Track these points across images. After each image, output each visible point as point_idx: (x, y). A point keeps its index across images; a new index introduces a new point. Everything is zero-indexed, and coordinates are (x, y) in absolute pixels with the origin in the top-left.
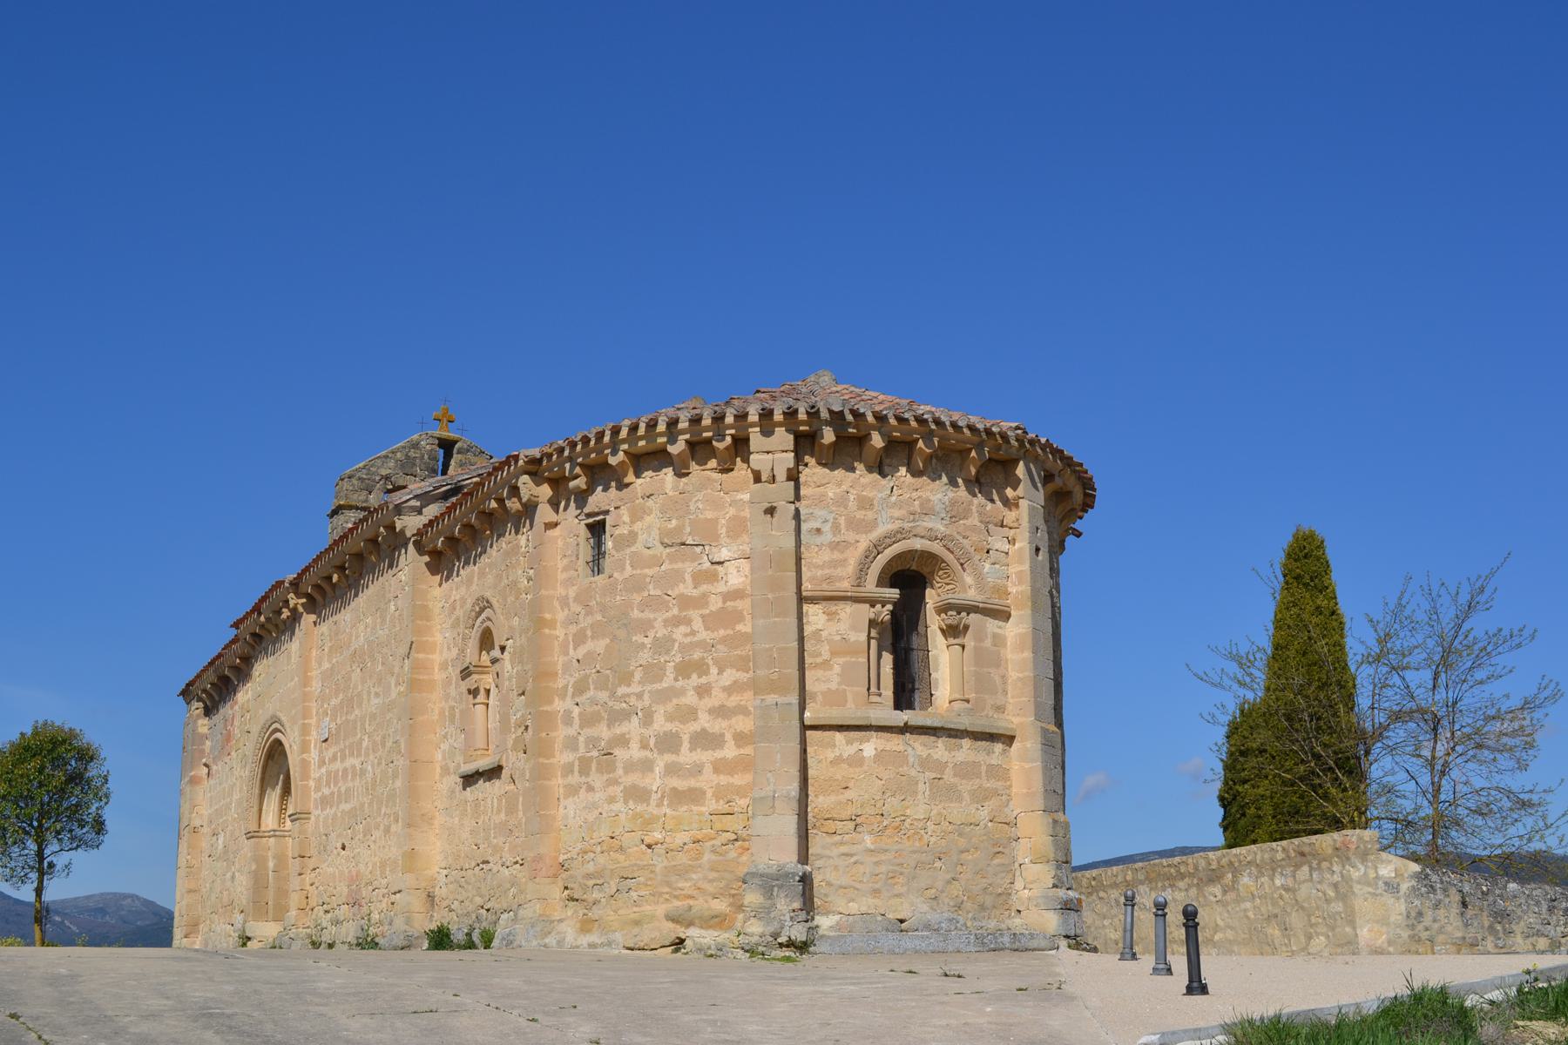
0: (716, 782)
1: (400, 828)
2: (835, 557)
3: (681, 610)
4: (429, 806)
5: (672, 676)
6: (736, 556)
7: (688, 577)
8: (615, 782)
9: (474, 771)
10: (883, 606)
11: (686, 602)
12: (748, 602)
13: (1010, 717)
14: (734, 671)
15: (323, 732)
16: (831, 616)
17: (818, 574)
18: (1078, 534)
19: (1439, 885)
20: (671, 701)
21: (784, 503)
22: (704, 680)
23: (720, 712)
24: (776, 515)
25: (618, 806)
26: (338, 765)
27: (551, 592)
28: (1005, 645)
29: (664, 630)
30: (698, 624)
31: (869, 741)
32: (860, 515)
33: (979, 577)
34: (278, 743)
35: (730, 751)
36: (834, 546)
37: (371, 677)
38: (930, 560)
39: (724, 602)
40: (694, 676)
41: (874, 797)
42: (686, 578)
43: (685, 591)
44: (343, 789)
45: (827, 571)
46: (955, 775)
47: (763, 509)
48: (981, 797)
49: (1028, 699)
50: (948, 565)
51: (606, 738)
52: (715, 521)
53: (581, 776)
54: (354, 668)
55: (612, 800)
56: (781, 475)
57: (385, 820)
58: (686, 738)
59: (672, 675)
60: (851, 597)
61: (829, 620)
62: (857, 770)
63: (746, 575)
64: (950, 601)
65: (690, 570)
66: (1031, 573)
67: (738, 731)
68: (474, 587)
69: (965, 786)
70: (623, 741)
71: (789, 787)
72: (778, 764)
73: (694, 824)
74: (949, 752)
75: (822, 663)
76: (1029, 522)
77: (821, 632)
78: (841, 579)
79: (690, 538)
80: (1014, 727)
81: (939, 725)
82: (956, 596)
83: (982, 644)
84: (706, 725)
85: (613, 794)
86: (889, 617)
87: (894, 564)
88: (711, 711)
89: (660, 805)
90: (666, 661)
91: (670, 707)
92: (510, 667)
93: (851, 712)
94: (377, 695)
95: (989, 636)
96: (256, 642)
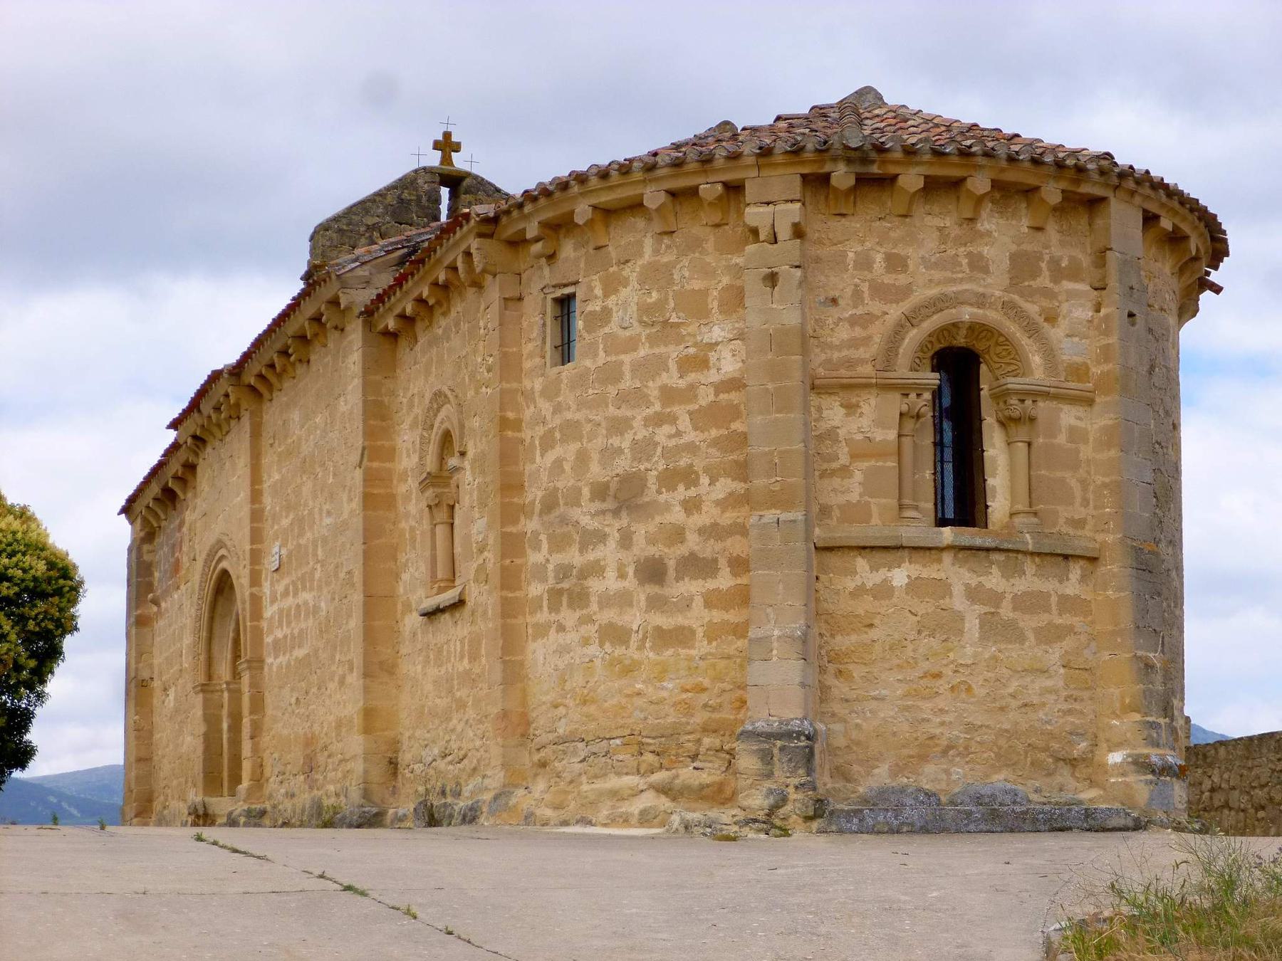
0: (707, 619)
1: (355, 679)
3: (663, 406)
4: (389, 651)
5: (654, 488)
7: (673, 366)
8: (589, 620)
9: (435, 607)
10: (919, 395)
11: (669, 395)
14: (729, 481)
15: (273, 559)
16: (851, 408)
18: (1217, 289)
20: (653, 519)
22: (692, 492)
25: (593, 649)
26: (290, 601)
27: (515, 385)
29: (644, 431)
30: (684, 423)
31: (899, 567)
32: (888, 279)
33: (1050, 354)
34: (225, 573)
36: (853, 321)
37: (322, 490)
39: (716, 395)
40: (681, 488)
42: (671, 367)
44: (296, 632)
45: (845, 353)
46: (1015, 609)
47: (761, 277)
50: (1007, 340)
51: (579, 565)
52: (705, 293)
53: (550, 613)
54: (305, 479)
55: (586, 642)
56: (784, 232)
57: (340, 669)
58: (671, 564)
60: (876, 384)
61: (847, 415)
63: (743, 360)
67: (735, 555)
68: (432, 379)
69: (1029, 623)
70: (596, 569)
72: (780, 597)
73: (681, 672)
84: (696, 548)
85: (586, 635)
88: (701, 531)
89: (641, 647)
90: (647, 470)
91: (652, 527)
92: (471, 479)
93: (877, 528)
94: (329, 513)
95: (1063, 430)
96: (198, 447)
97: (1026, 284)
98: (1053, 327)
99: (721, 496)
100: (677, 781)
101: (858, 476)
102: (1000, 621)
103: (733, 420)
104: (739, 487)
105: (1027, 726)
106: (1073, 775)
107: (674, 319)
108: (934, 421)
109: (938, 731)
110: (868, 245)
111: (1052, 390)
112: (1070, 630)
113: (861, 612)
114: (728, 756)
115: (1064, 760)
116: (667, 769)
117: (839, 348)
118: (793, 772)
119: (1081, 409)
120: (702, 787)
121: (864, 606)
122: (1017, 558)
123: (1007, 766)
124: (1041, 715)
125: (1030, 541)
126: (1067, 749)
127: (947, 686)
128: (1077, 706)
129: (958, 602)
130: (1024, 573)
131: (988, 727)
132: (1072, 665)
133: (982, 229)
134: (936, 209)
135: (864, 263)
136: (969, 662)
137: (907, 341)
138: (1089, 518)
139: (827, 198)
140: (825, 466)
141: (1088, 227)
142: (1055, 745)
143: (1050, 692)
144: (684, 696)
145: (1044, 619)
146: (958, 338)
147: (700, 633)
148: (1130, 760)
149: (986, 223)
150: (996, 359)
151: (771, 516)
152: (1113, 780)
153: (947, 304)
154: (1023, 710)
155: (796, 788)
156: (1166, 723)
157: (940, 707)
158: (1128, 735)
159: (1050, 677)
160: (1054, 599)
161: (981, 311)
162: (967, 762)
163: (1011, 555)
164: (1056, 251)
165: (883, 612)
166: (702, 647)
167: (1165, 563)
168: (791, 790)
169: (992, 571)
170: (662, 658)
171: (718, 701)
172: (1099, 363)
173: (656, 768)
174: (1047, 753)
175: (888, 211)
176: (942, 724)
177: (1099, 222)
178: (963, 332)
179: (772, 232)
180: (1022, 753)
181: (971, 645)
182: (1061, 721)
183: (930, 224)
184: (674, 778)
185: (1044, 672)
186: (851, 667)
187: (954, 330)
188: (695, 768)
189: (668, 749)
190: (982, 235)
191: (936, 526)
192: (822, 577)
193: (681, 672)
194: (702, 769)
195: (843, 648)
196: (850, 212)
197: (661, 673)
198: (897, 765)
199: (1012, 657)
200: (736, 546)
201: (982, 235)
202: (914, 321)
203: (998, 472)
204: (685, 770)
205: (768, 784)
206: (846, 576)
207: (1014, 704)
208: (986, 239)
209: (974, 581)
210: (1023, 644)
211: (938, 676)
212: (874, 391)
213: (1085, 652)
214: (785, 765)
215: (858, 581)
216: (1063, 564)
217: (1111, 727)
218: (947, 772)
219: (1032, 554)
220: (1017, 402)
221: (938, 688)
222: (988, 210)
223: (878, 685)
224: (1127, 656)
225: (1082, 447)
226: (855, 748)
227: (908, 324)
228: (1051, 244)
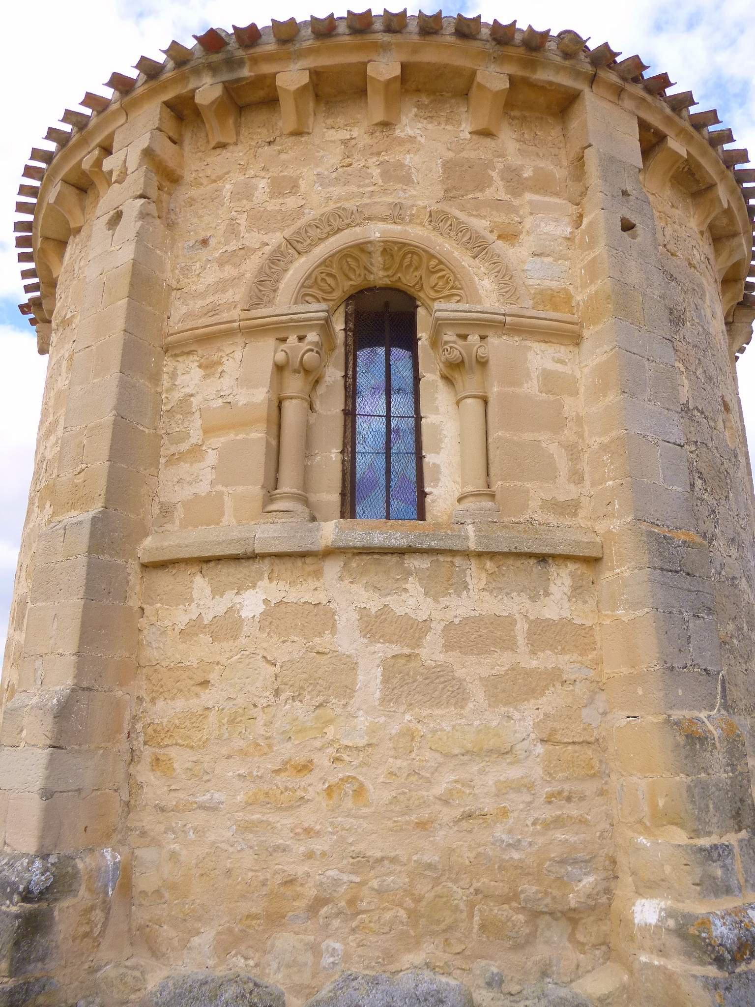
2: (225, 274)
10: (301, 339)
16: (210, 367)
31: (254, 587)
32: (273, 205)
49: (619, 482)
50: (441, 262)
60: (240, 329)
62: (226, 645)
74: (436, 600)
75: (189, 452)
77: (192, 399)
83: (517, 390)
95: (534, 376)
97: (470, 196)
98: (513, 245)
101: (211, 457)
102: (422, 670)
105: (472, 855)
106: (572, 938)
108: (346, 382)
109: (301, 870)
110: (251, 173)
111: (508, 319)
112: (555, 677)
113: (193, 661)
115: (551, 914)
117: (202, 295)
119: (563, 348)
122: (452, 562)
123: (433, 934)
124: (499, 832)
126: (555, 892)
127: (321, 787)
128: (573, 810)
130: (466, 587)
131: (394, 860)
132: (558, 737)
133: (402, 135)
134: (341, 121)
135: (245, 192)
136: (362, 742)
137: (291, 272)
138: (584, 500)
140: (173, 449)
141: (561, 138)
142: (529, 889)
143: (517, 790)
145: (503, 661)
146: (375, 270)
150: (433, 294)
152: (644, 958)
153: (347, 221)
154: (465, 824)
156: (741, 841)
157: (306, 825)
158: (668, 869)
159: (516, 762)
160: (521, 628)
161: (399, 227)
163: (441, 558)
164: (514, 160)
167: (727, 569)
169: (407, 586)
172: (584, 286)
174: (514, 904)
176: (310, 855)
177: (574, 125)
178: (378, 259)
180: (462, 906)
181: (367, 712)
182: (540, 840)
183: (333, 139)
185: (505, 752)
186: (173, 752)
187: (364, 258)
190: (401, 142)
192: (148, 609)
195: (165, 720)
198: (230, 931)
199: (442, 730)
201: (401, 142)
202: (299, 247)
203: (443, 446)
208: (408, 146)
209: (374, 603)
210: (462, 708)
211: (305, 768)
212: (240, 340)
213: (585, 712)
216: (538, 569)
217: (637, 849)
218: (314, 949)
219: (480, 555)
220: (454, 338)
221: (305, 790)
222: (411, 115)
223: (209, 784)
224: (655, 721)
225: (568, 402)
226: (167, 895)
227: (292, 251)
228: (508, 153)
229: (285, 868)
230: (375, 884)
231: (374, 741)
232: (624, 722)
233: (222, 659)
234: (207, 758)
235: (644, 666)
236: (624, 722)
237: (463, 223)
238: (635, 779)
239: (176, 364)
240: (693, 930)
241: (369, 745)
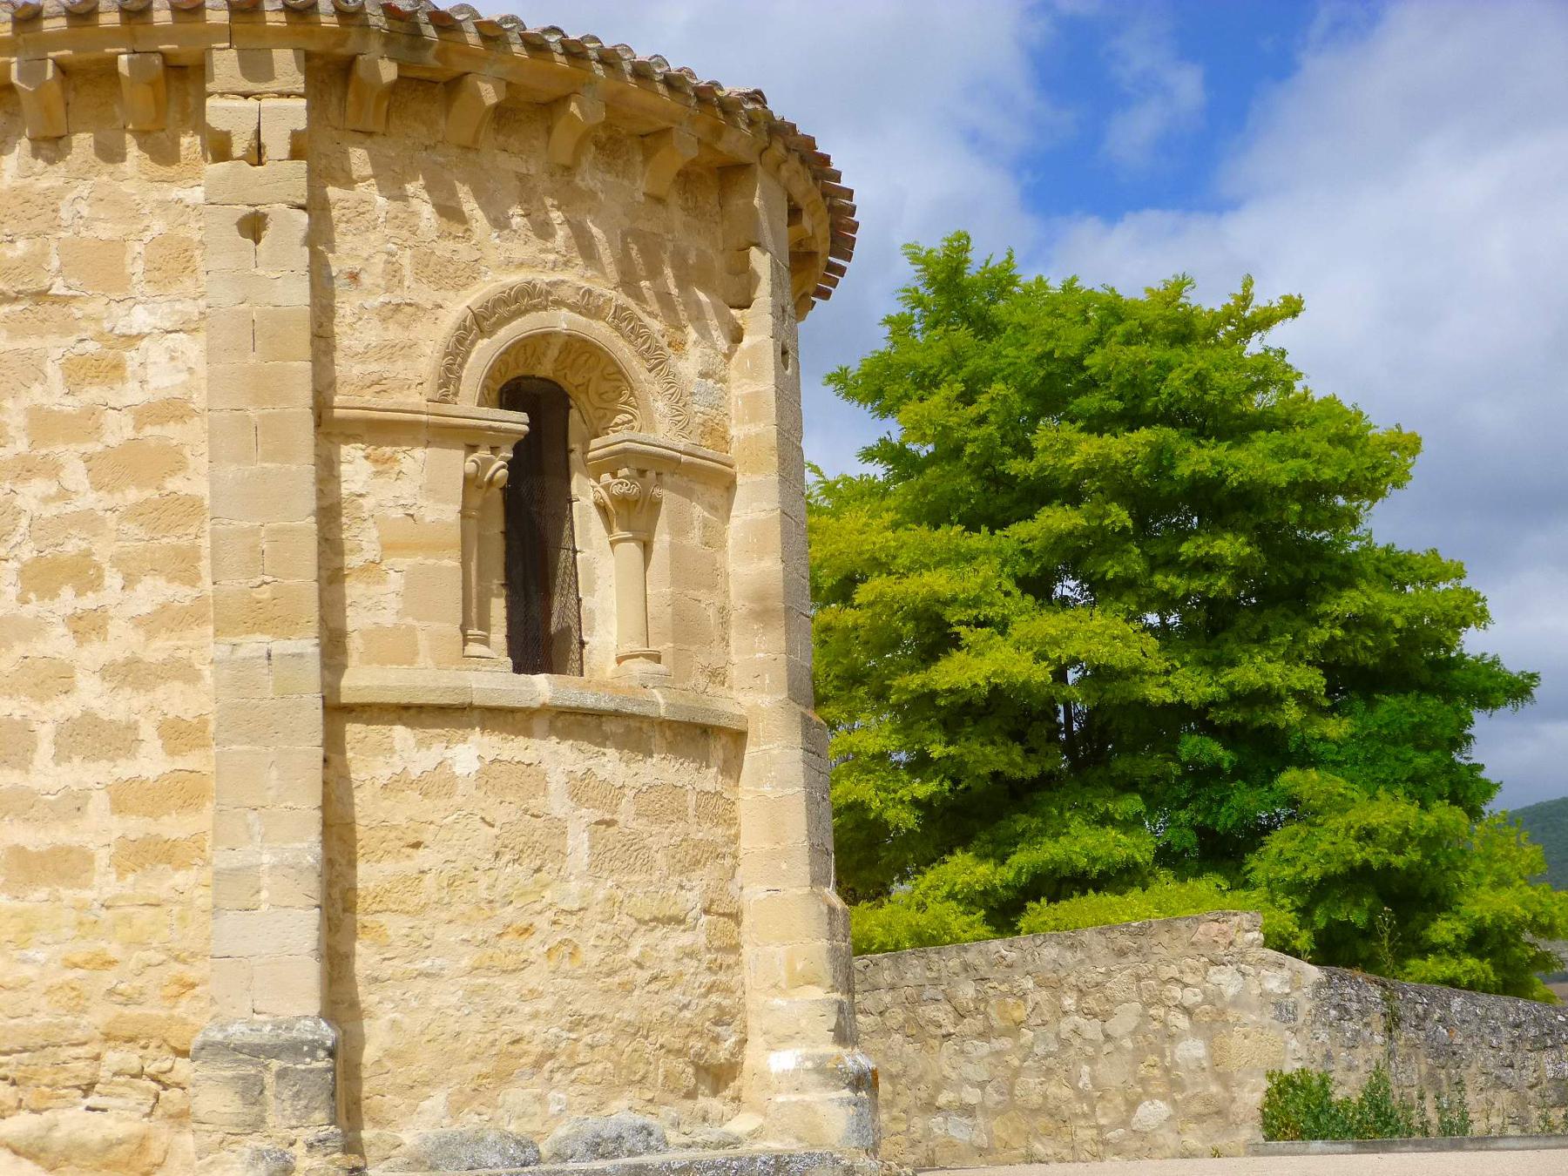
6: (168, 325)
7: (53, 370)
11: (43, 424)
12: (197, 426)
13: (734, 694)
14: (161, 582)
17: (354, 372)
19: (1355, 1006)
21: (284, 206)
22: (89, 601)
23: (128, 673)
24: (267, 236)
28: (723, 546)
30: (75, 475)
31: (465, 741)
35: (151, 762)
38: (584, 358)
39: (138, 427)
40: (67, 592)
41: (477, 863)
43: (47, 402)
48: (690, 860)
56: (277, 145)
58: (46, 733)
59: (11, 588)
61: (378, 473)
62: (441, 803)
64: (627, 445)
65: (58, 353)
66: (778, 399)
69: (659, 838)
71: (298, 845)
72: (271, 793)
76: (773, 294)
77: (361, 500)
78: (406, 386)
79: (59, 281)
80: (743, 712)
81: (611, 706)
82: (634, 435)
84: (96, 704)
86: (504, 472)
87: (511, 360)
99: (146, 609)
100: (57, 1134)
101: (395, 581)
103: (173, 473)
104: (182, 594)
107: (58, 289)
109: (527, 1029)
111: (684, 458)
113: (400, 819)
114: (154, 1085)
116: (34, 1111)
118: (303, 1119)
120: (109, 1145)
121: (406, 810)
123: (631, 1083)
125: (661, 701)
129: (557, 803)
131: (602, 1018)
133: (581, 184)
136: (576, 907)
139: (343, 98)
141: (718, 208)
144: (70, 975)
147: (102, 857)
148: (809, 1065)
149: (588, 177)
151: (255, 646)
155: (311, 1146)
158: (803, 1023)
162: (572, 1081)
165: (438, 821)
166: (105, 883)
168: (299, 1150)
170: (26, 904)
171: (138, 983)
173: (10, 1108)
175: (440, 137)
176: (535, 1015)
178: (553, 352)
179: (254, 144)
184: (50, 1129)
185: (679, 921)
186: (383, 918)
188: (88, 1109)
189: (35, 1072)
191: (518, 669)
193: (65, 930)
194: (104, 1110)
196: (380, 128)
197: (22, 932)
200: (178, 701)
204: (69, 1113)
205: (254, 1142)
206: (376, 755)
207: (642, 976)
211: (526, 931)
214: (287, 1104)
215: (397, 764)
218: (540, 1099)
229: (514, 1027)
230: (588, 1039)
231: (584, 905)
232: (763, 895)
233: (436, 817)
234: (426, 923)
235: (790, 842)
236: (763, 895)
237: (645, 327)
238: (772, 947)
239: (330, 446)
240: (830, 1065)
241: (580, 910)
